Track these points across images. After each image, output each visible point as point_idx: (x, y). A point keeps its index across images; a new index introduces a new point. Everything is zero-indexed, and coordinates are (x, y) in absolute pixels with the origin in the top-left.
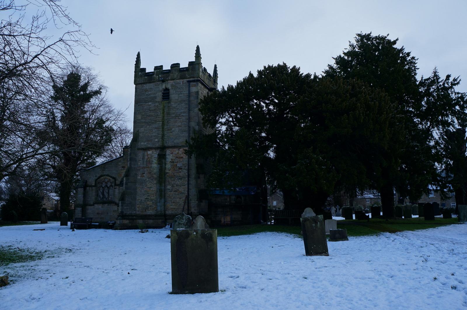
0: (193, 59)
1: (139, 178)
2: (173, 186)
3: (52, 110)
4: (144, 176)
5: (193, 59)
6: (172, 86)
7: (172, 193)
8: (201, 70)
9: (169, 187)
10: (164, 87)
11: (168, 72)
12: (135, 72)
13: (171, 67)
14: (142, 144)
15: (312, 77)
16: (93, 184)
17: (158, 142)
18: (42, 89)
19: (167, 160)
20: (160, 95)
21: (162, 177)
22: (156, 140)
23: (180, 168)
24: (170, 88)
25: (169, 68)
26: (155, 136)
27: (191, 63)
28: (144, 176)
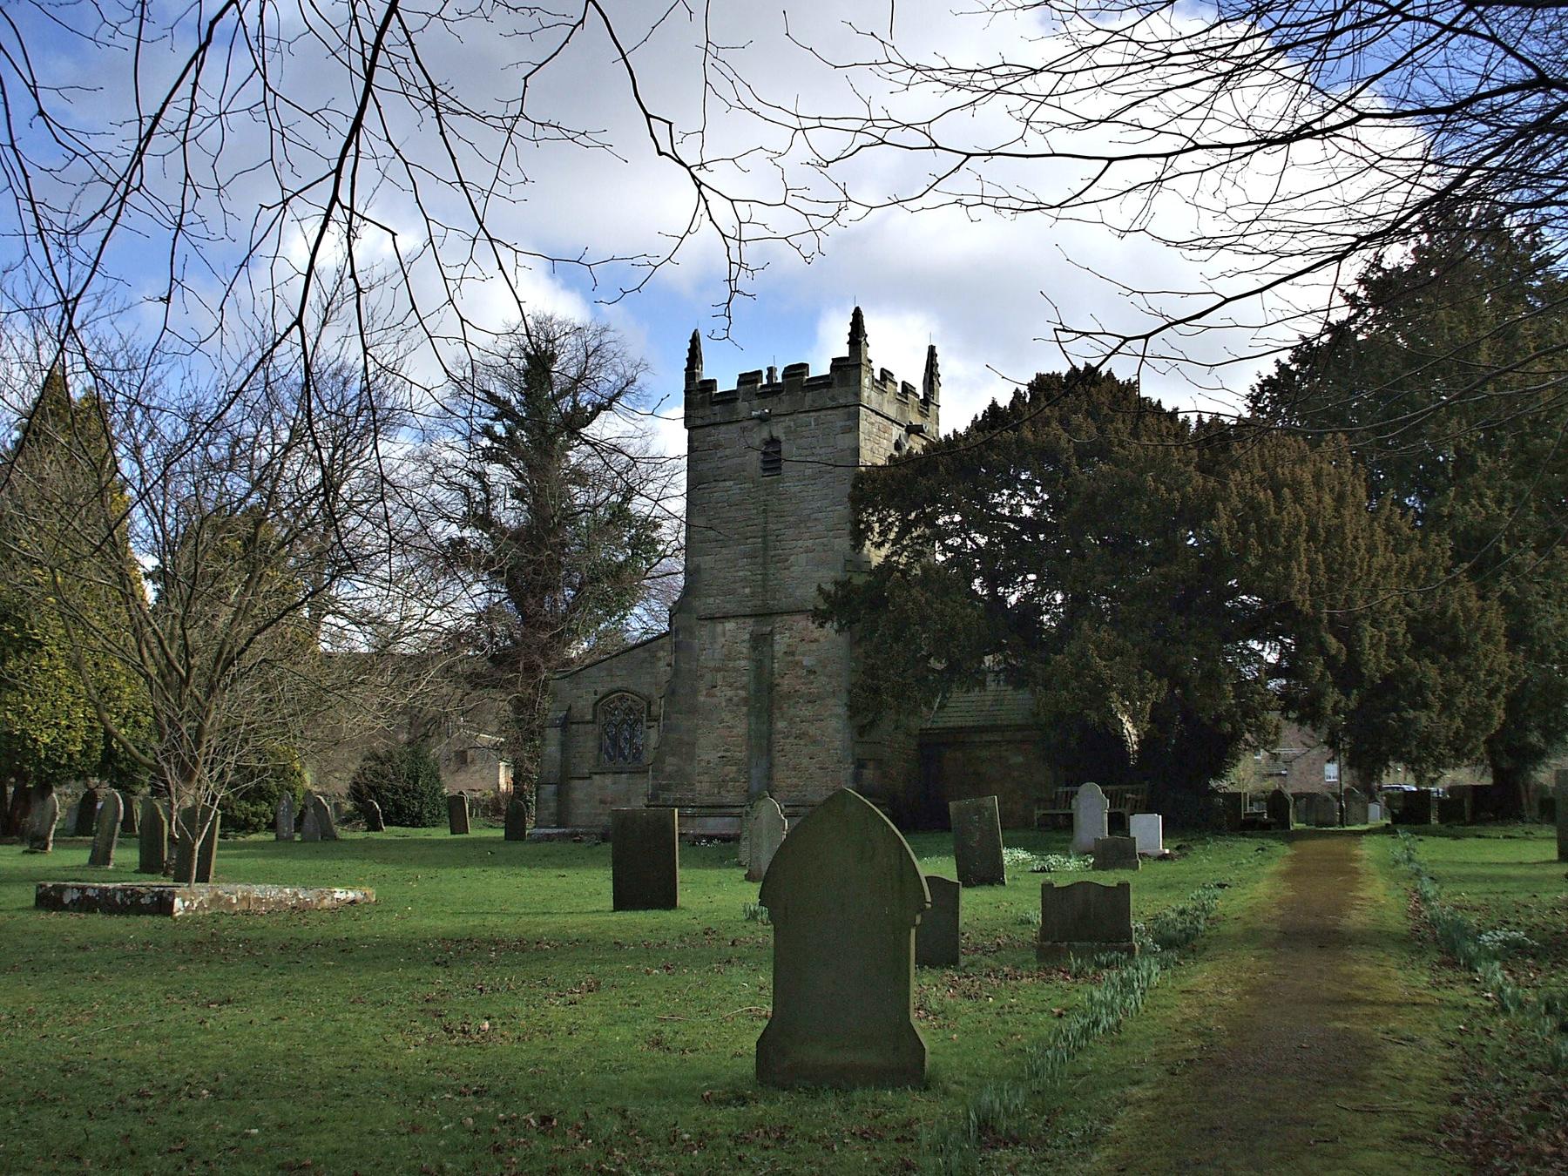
0: (844, 352)
1: (702, 699)
2: (791, 721)
3: (1371, 311)
4: (714, 696)
5: (844, 352)
6: (788, 431)
7: (791, 740)
8: (866, 382)
9: (781, 725)
10: (765, 435)
11: (729, 397)
12: (686, 392)
13: (739, 383)
14: (711, 603)
15: (396, 606)
16: (589, 717)
17: (753, 594)
18: (422, 455)
19: (776, 647)
20: (755, 458)
21: (764, 698)
22: (747, 590)
23: (811, 672)
24: (783, 438)
25: (731, 385)
26: (744, 579)
27: (837, 363)
28: (714, 696)
